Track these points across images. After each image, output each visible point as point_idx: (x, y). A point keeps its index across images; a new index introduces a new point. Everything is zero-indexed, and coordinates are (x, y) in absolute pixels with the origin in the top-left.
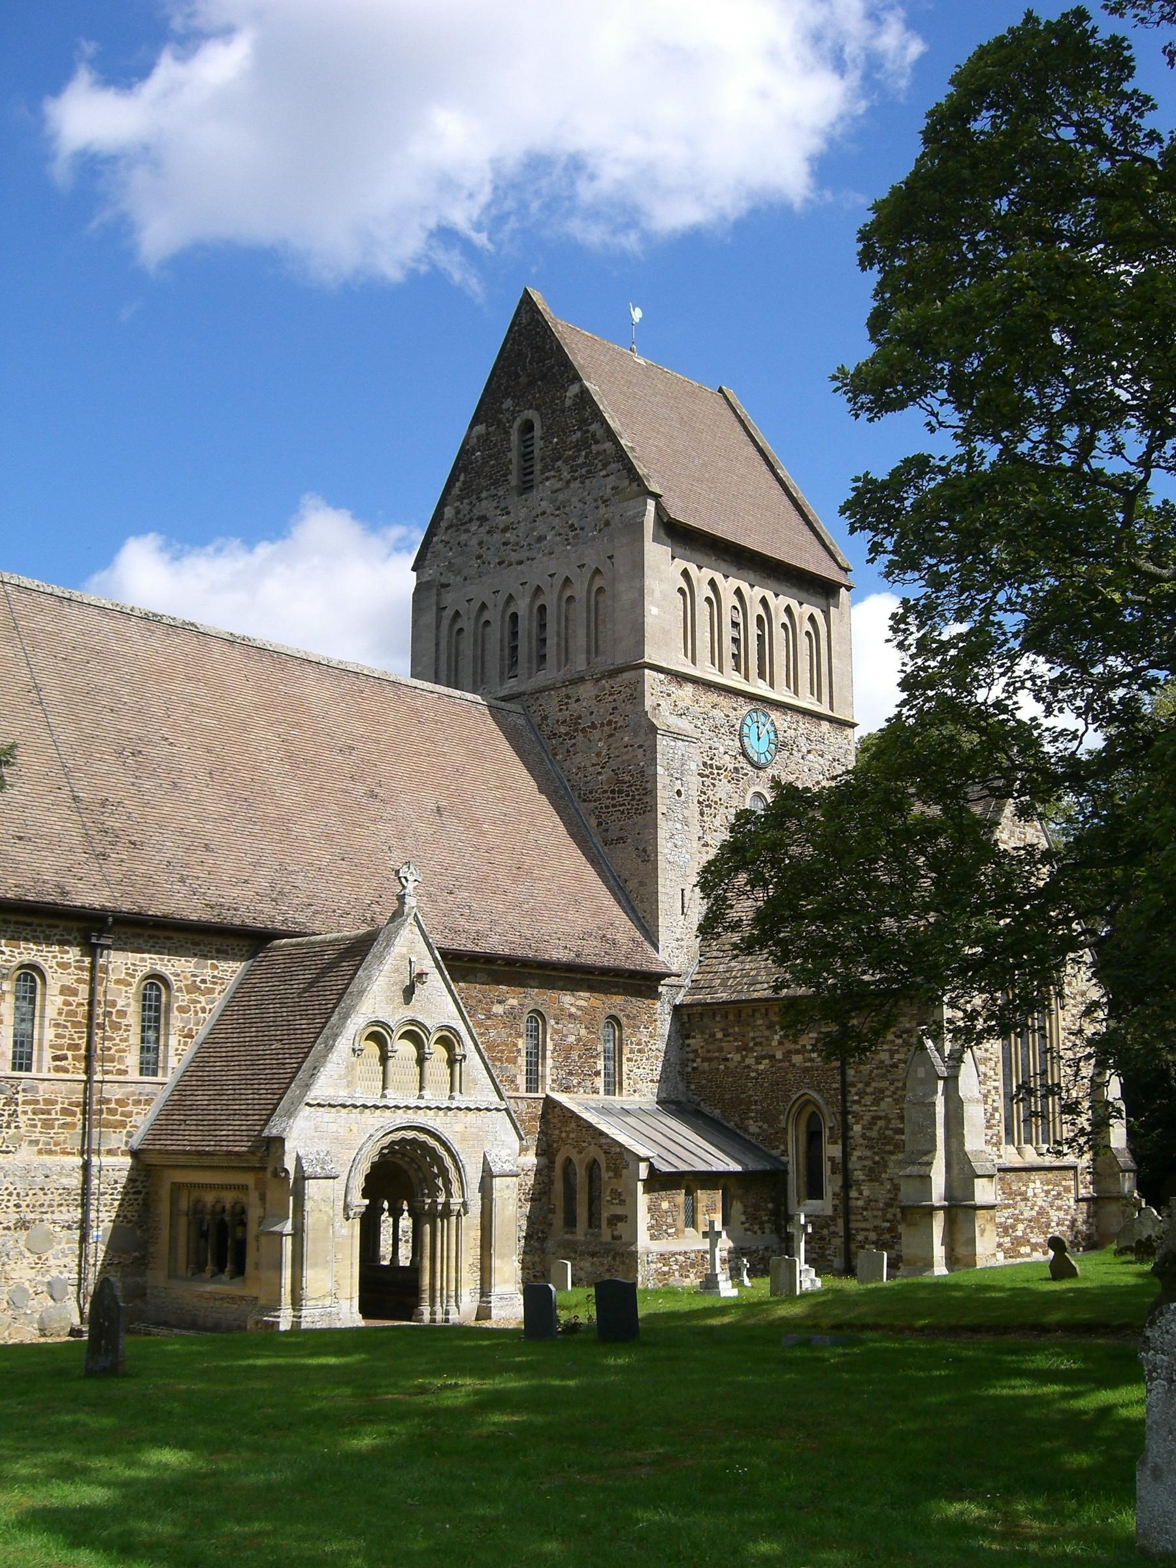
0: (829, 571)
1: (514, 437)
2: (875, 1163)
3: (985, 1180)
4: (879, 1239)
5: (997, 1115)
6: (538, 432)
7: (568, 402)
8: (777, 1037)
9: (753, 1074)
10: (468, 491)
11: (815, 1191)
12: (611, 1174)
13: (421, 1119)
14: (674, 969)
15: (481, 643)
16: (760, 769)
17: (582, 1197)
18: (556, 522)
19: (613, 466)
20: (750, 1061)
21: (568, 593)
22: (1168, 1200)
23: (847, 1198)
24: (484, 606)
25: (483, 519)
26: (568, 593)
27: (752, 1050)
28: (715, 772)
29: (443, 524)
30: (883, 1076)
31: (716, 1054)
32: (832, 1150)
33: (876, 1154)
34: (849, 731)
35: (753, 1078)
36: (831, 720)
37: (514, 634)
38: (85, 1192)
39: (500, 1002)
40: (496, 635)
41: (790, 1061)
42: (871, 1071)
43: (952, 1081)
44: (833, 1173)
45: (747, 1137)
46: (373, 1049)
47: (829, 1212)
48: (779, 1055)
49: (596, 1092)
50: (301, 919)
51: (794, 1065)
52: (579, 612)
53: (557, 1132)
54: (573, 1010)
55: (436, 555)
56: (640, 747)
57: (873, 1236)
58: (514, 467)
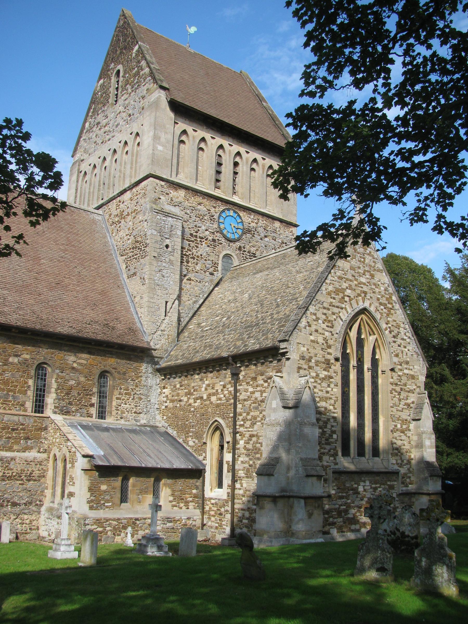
2: (250, 466)
3: (315, 479)
4: (250, 517)
5: (335, 436)
8: (204, 386)
9: (192, 409)
12: (70, 465)
16: (231, 241)
20: (191, 401)
27: (192, 394)
28: (199, 240)
29: (85, 131)
30: (256, 408)
31: (176, 398)
32: (228, 457)
33: (250, 459)
34: (294, 229)
35: (192, 412)
36: (281, 221)
39: (17, 356)
41: (210, 400)
42: (250, 405)
44: (228, 472)
45: (188, 448)
48: (205, 397)
49: (90, 416)
51: (211, 403)
53: (52, 438)
54: (75, 365)
56: (146, 221)
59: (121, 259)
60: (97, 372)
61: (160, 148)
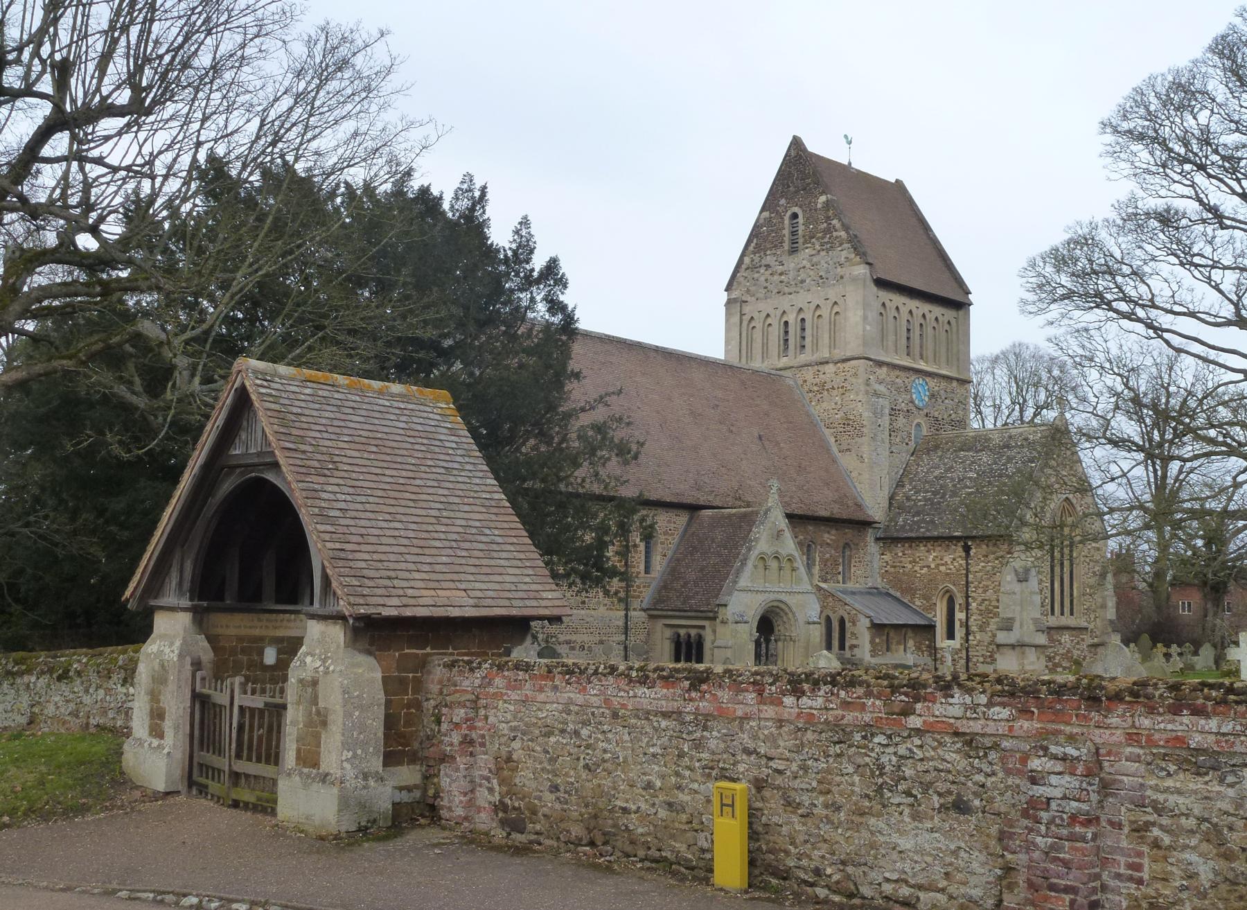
0: (958, 297)
1: (787, 221)
6: (801, 220)
7: (819, 206)
10: (758, 249)
11: (951, 636)
13: (783, 597)
14: (876, 519)
15: (765, 336)
17: (836, 635)
18: (812, 273)
19: (846, 245)
20: (917, 568)
21: (818, 313)
22: (435, 198)
23: (967, 641)
24: (768, 315)
25: (768, 266)
26: (818, 313)
29: (744, 266)
32: (960, 616)
36: (958, 380)
37: (786, 332)
38: (626, 628)
40: (775, 333)
43: (66, 8)
46: (761, 565)
47: (958, 646)
48: (933, 566)
50: (710, 498)
52: (825, 322)
55: (739, 283)
57: (981, 659)
58: (786, 239)
59: (827, 432)
60: (841, 545)
61: (868, 328)
